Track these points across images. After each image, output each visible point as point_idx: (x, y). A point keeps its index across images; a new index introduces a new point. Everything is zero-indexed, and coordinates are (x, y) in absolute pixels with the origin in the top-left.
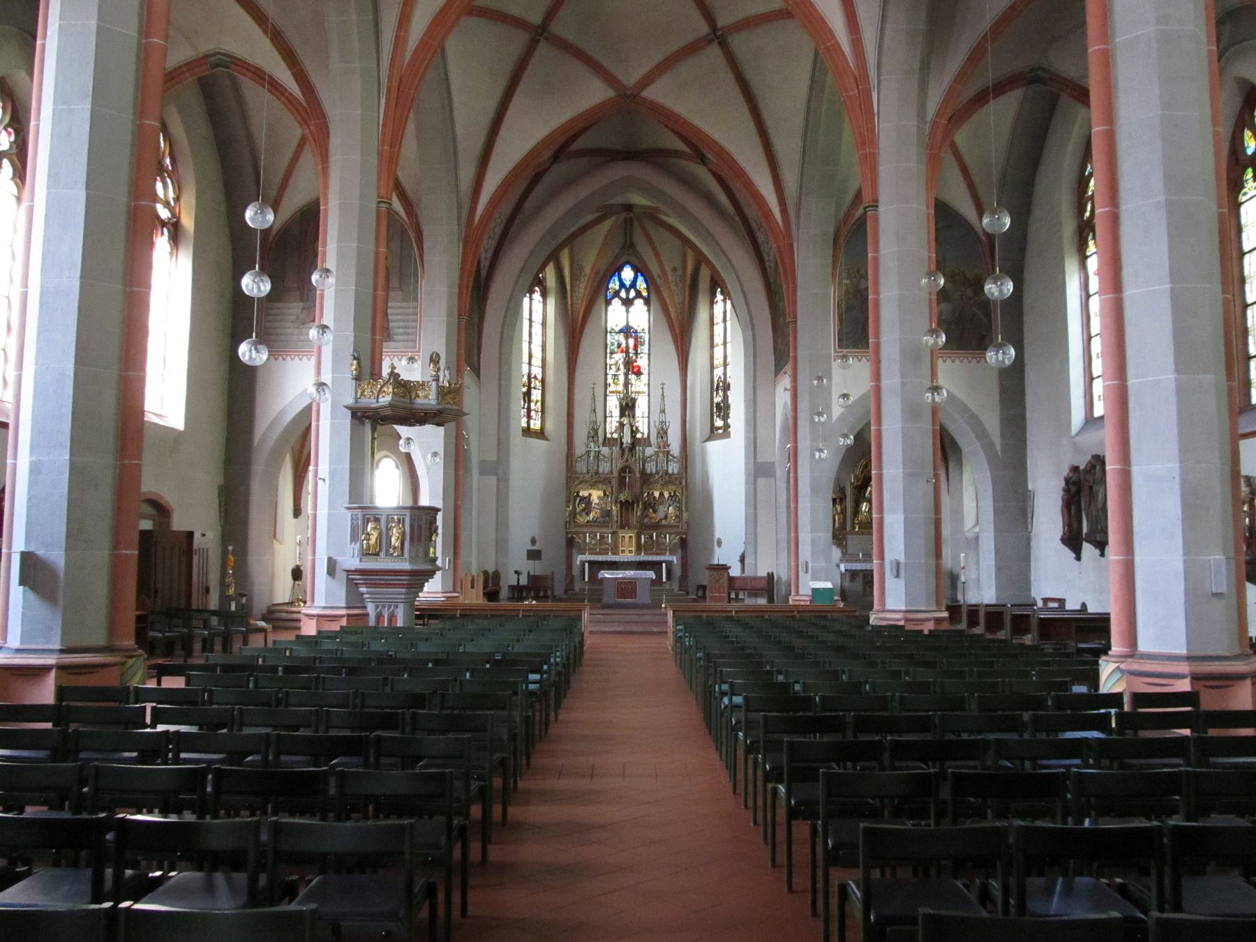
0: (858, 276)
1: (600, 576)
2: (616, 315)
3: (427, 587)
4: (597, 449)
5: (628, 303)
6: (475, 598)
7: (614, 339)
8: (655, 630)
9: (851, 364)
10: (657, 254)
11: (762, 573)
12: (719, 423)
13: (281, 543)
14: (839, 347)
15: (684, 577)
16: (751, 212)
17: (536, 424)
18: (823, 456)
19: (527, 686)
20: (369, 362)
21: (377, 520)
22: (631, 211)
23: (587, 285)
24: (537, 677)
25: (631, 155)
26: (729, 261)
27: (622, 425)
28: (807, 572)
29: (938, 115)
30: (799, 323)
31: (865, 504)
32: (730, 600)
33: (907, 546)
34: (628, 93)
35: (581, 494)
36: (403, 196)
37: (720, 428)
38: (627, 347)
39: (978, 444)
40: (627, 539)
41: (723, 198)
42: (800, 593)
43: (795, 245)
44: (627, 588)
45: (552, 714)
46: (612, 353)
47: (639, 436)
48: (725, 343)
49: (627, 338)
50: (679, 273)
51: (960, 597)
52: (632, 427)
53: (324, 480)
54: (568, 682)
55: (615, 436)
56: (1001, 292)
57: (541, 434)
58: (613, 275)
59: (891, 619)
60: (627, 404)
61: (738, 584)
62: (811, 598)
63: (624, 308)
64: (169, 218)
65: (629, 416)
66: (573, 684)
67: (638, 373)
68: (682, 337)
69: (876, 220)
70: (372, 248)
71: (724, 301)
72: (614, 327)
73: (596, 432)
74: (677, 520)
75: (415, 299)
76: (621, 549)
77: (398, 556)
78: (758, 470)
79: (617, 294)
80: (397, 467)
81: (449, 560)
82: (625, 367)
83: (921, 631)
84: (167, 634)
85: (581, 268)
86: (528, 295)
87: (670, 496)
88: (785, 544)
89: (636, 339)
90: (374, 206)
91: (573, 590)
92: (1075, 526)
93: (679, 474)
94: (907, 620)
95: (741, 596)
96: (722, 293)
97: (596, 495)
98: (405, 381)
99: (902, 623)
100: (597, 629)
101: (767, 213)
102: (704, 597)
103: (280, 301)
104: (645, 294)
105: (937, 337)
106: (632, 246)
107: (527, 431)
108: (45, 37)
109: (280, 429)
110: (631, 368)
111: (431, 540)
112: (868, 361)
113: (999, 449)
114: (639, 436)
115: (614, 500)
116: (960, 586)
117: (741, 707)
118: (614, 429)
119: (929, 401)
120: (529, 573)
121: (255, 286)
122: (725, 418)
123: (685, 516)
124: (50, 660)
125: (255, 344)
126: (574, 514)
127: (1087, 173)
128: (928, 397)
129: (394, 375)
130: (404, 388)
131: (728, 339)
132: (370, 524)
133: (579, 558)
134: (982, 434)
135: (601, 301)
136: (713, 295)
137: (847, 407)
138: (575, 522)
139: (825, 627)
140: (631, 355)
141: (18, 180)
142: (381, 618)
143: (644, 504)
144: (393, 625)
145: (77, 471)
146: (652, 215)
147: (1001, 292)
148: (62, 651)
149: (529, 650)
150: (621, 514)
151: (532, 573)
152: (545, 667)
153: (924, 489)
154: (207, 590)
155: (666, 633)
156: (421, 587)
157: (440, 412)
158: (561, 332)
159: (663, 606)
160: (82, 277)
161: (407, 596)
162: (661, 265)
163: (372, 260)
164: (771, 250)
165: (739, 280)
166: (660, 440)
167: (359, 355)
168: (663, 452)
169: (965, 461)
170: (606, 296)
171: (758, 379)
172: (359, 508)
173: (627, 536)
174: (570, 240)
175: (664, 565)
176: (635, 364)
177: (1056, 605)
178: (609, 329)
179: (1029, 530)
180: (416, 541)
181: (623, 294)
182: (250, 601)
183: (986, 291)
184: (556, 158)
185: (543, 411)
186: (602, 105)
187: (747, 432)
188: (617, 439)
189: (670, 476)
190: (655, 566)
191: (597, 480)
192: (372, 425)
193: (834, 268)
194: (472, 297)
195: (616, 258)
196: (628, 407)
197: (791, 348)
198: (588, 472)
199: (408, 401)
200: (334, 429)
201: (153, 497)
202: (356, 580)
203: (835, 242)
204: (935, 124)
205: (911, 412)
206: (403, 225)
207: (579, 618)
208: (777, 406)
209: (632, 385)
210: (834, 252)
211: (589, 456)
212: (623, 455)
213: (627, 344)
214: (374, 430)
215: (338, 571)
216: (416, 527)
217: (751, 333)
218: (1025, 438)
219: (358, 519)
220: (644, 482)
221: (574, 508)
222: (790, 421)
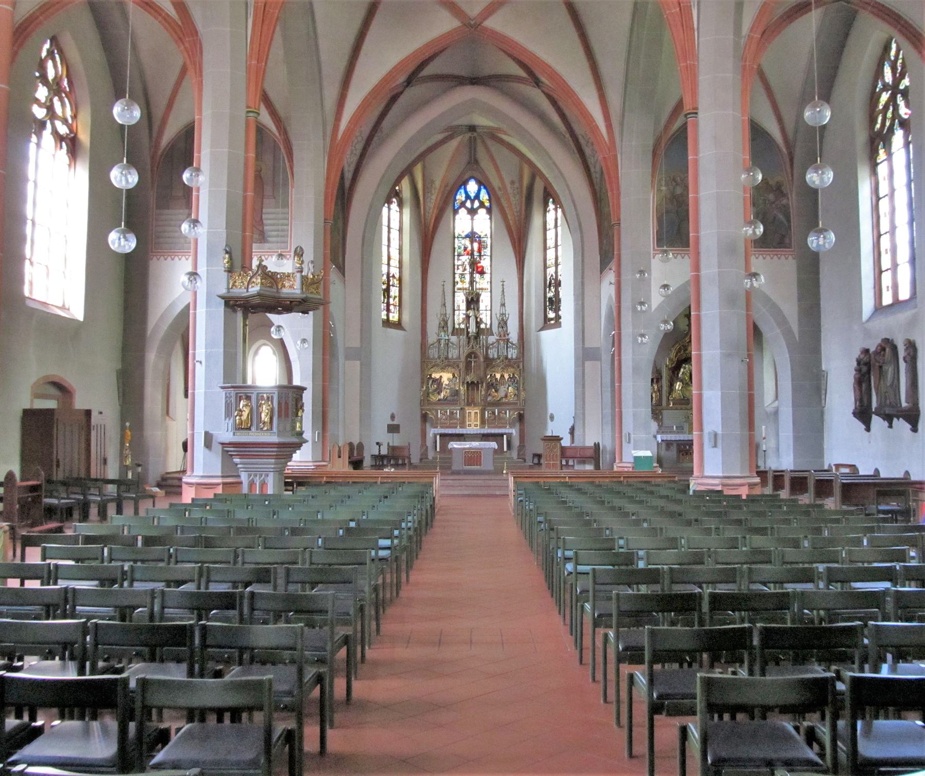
0: (674, 184)
1: (450, 446)
2: (462, 223)
3: (297, 456)
5: (472, 212)
6: (342, 466)
8: (498, 493)
11: (590, 443)
12: (551, 315)
13: (173, 420)
14: (658, 246)
15: (522, 446)
17: (394, 317)
18: (645, 340)
19: (377, 553)
21: (248, 398)
23: (436, 198)
24: (387, 543)
25: (475, 81)
27: (468, 317)
28: (629, 442)
29: (752, 30)
30: (622, 225)
31: (678, 383)
32: (562, 466)
34: (472, 23)
35: (433, 376)
36: (273, 113)
37: (552, 319)
38: (472, 250)
39: (778, 331)
40: (473, 414)
41: (556, 118)
42: (624, 460)
44: (473, 457)
45: (404, 576)
46: (459, 255)
47: (483, 326)
48: (556, 246)
49: (472, 243)
50: (517, 185)
51: (761, 463)
52: (476, 318)
53: (201, 362)
54: (419, 543)
55: (463, 326)
56: (822, 180)
57: (398, 325)
58: (460, 188)
59: (708, 485)
60: (472, 299)
61: (568, 453)
62: (633, 465)
63: (469, 217)
64: (67, 134)
66: (425, 546)
67: (482, 273)
69: (696, 125)
70: (241, 153)
71: (556, 209)
73: (446, 323)
74: (516, 398)
75: (286, 205)
77: (267, 430)
79: (463, 204)
80: (274, 353)
81: (318, 433)
82: (470, 268)
83: (739, 496)
84: (63, 501)
85: (433, 182)
86: (386, 205)
87: (510, 377)
88: (610, 418)
89: (480, 243)
90: (243, 115)
91: (427, 458)
92: (865, 400)
93: (517, 358)
94: (723, 485)
95: (571, 463)
96: (554, 202)
97: (446, 377)
98: (272, 273)
99: (719, 488)
100: (446, 492)
101: (595, 129)
102: (539, 464)
104: (487, 204)
105: (755, 228)
106: (476, 162)
107: (387, 323)
110: (476, 268)
111: (297, 415)
112: (794, 259)
114: (483, 326)
115: (461, 381)
116: (761, 453)
117: (588, 574)
118: (461, 320)
120: (388, 444)
121: (123, 178)
122: (556, 310)
125: (124, 233)
127: (878, 90)
128: (747, 283)
129: (262, 267)
130: (271, 278)
131: (559, 243)
132: (242, 402)
133: (431, 432)
134: (782, 321)
135: (449, 211)
136: (546, 205)
137: (667, 297)
139: (652, 493)
142: (253, 486)
144: (264, 492)
146: (493, 135)
147: (822, 180)
149: (381, 517)
152: (396, 532)
153: (737, 368)
154: (105, 461)
156: (290, 457)
158: (415, 238)
159: (505, 472)
161: (276, 466)
162: (501, 179)
163: (242, 165)
164: (596, 159)
167: (231, 249)
168: (504, 340)
169: (765, 345)
171: (586, 281)
172: (233, 387)
175: (505, 436)
176: (479, 265)
177: (847, 470)
179: (823, 405)
180: (283, 416)
181: (468, 204)
182: (146, 470)
183: (807, 180)
184: (409, 82)
186: (449, 34)
187: (576, 322)
188: (463, 329)
190: (497, 437)
191: (447, 364)
192: (243, 313)
193: (653, 176)
194: (336, 204)
195: (463, 173)
196: (473, 301)
198: (439, 357)
199: (275, 290)
200: (209, 316)
201: (57, 380)
203: (654, 153)
204: (750, 38)
205: (729, 299)
206: (275, 141)
207: (431, 484)
208: (602, 300)
209: (476, 282)
210: (653, 161)
212: (469, 342)
214: (245, 318)
216: (283, 405)
218: (820, 325)
219: (231, 397)
221: (428, 388)
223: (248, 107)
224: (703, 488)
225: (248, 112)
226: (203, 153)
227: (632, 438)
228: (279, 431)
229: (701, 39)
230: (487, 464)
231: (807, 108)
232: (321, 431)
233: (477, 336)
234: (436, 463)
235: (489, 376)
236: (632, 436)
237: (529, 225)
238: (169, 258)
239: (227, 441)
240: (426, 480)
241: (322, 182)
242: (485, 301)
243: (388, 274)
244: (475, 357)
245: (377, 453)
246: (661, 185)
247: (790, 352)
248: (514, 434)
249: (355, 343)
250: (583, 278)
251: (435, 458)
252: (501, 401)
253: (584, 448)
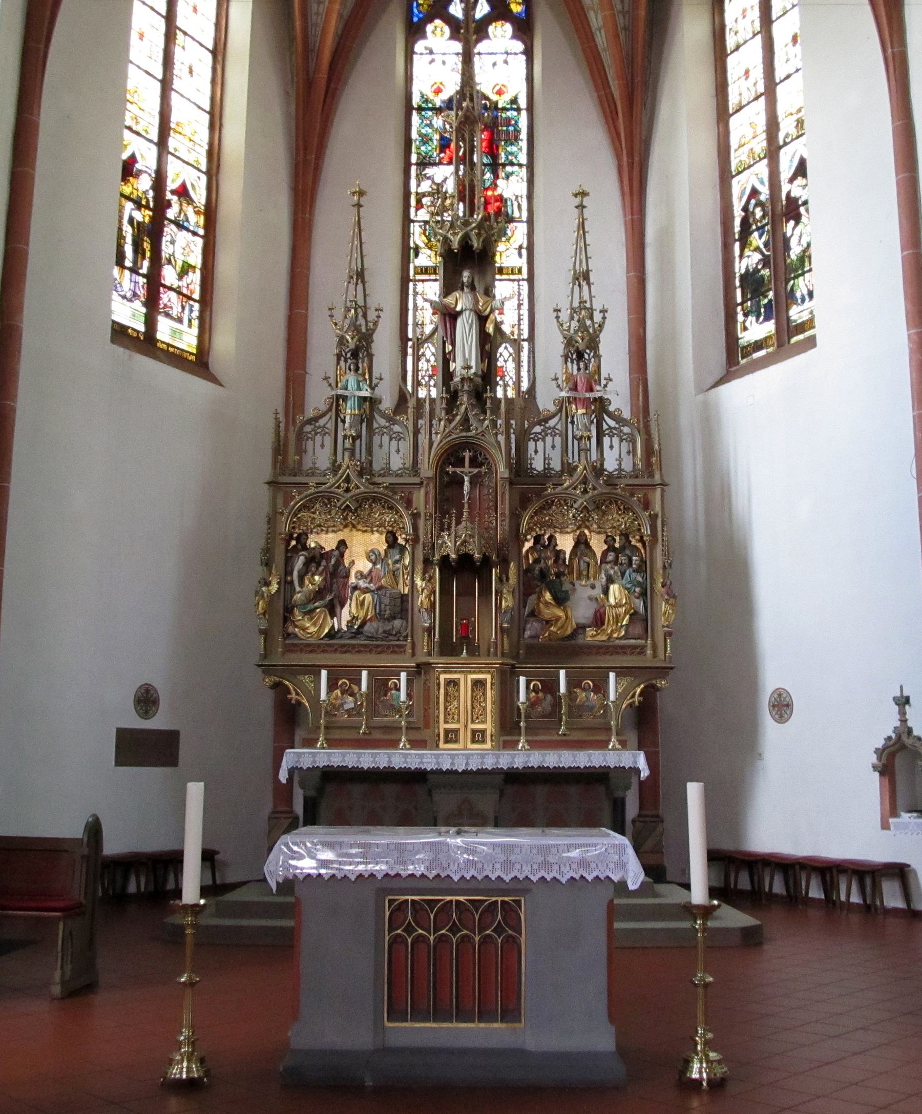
4: (366, 393)
46: (423, 163)
52: (482, 319)
65: (472, 288)
68: (630, 100)
72: (431, 96)
74: (638, 629)
76: (443, 726)
87: (611, 548)
115: (420, 556)
138: (287, 635)
143: (526, 573)
159: (698, 1070)
166: (573, 368)
168: (586, 403)
173: (466, 681)
175: (324, 673)
178: (416, 100)
185: (206, 300)
189: (611, 480)
198: (335, 468)
211: (339, 417)
220: (524, 501)
221: (287, 585)
235: (528, 545)
252: (580, 640)
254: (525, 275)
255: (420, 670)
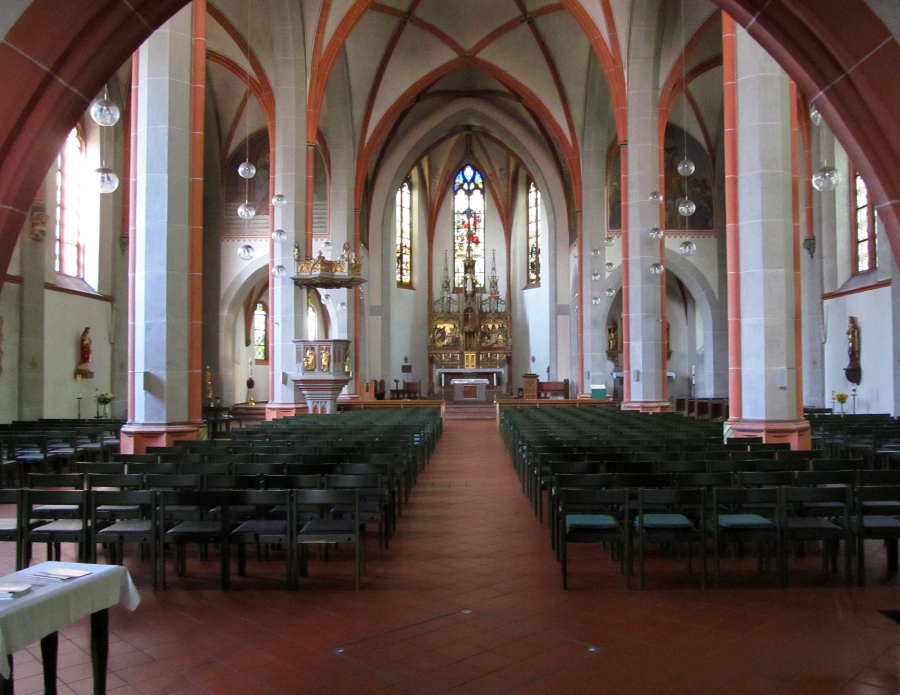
2: (460, 201)
5: (469, 193)
6: (369, 397)
7: (460, 218)
9: (613, 244)
10: (489, 159)
11: (561, 379)
12: (533, 276)
16: (551, 133)
17: (406, 279)
18: (598, 302)
20: (304, 247)
21: (313, 349)
22: (471, 130)
24: (418, 435)
25: (471, 94)
26: (538, 167)
27: (466, 279)
28: (589, 379)
33: (644, 361)
37: (533, 280)
38: (469, 225)
41: (534, 125)
43: (581, 159)
44: (470, 391)
46: (458, 228)
47: (478, 286)
48: (537, 221)
49: (469, 218)
50: (504, 172)
52: (473, 280)
53: (278, 324)
54: (433, 445)
55: (461, 286)
56: (688, 211)
57: (410, 286)
58: (458, 173)
59: (633, 407)
61: (545, 387)
63: (466, 196)
67: (477, 242)
70: (304, 176)
71: (536, 191)
72: (460, 210)
73: (448, 284)
75: (324, 198)
78: (558, 310)
79: (461, 187)
85: (436, 169)
87: (500, 328)
89: (475, 218)
91: (434, 392)
93: (505, 312)
94: (644, 407)
95: (548, 396)
96: (535, 186)
97: (448, 327)
101: (563, 137)
103: (234, 201)
104: (481, 186)
106: (472, 153)
107: (401, 284)
108: (137, 84)
109: (237, 288)
110: (472, 238)
113: (717, 296)
114: (478, 286)
118: (460, 281)
119: (653, 272)
120: (404, 381)
122: (537, 273)
123: (510, 341)
124: (163, 429)
126: (433, 341)
130: (328, 265)
131: (539, 219)
135: (450, 192)
136: (528, 188)
138: (434, 346)
140: (471, 230)
141: (80, 138)
144: (324, 413)
145: (171, 328)
147: (688, 211)
148: (168, 424)
150: (466, 340)
151: (406, 381)
155: (495, 419)
156: (340, 390)
157: (350, 280)
160: (168, 222)
162: (492, 168)
165: (545, 180)
166: (492, 289)
170: (454, 188)
173: (470, 356)
174: (428, 151)
175: (495, 375)
176: (474, 236)
181: (466, 186)
182: (222, 402)
183: (679, 211)
185: (411, 270)
188: (462, 288)
190: (489, 375)
191: (449, 317)
196: (470, 266)
197: (579, 230)
200: (284, 291)
202: (301, 386)
204: (664, 91)
207: (439, 409)
211: (443, 301)
212: (466, 300)
213: (469, 222)
214: (308, 292)
215: (289, 380)
216: (337, 353)
217: (553, 217)
221: (434, 336)
222: (579, 278)
223: (308, 142)
224: (741, 435)
225: (308, 146)
226: (276, 176)
227: (591, 375)
228: (334, 372)
229: (630, 92)
230: (481, 396)
231: (680, 164)
232: (354, 372)
233: (473, 294)
234: (442, 395)
235: (483, 327)
236: (591, 373)
237: (514, 205)
238: (236, 240)
239: (299, 379)
240: (437, 406)
241: (352, 182)
242: (479, 267)
243: (401, 244)
244: (472, 311)
245: (395, 388)
246: (614, 182)
247: (712, 309)
248: (503, 373)
249: (377, 302)
250: (555, 250)
251: (440, 392)
253: (557, 383)
254: (483, 256)
255: (462, 354)
